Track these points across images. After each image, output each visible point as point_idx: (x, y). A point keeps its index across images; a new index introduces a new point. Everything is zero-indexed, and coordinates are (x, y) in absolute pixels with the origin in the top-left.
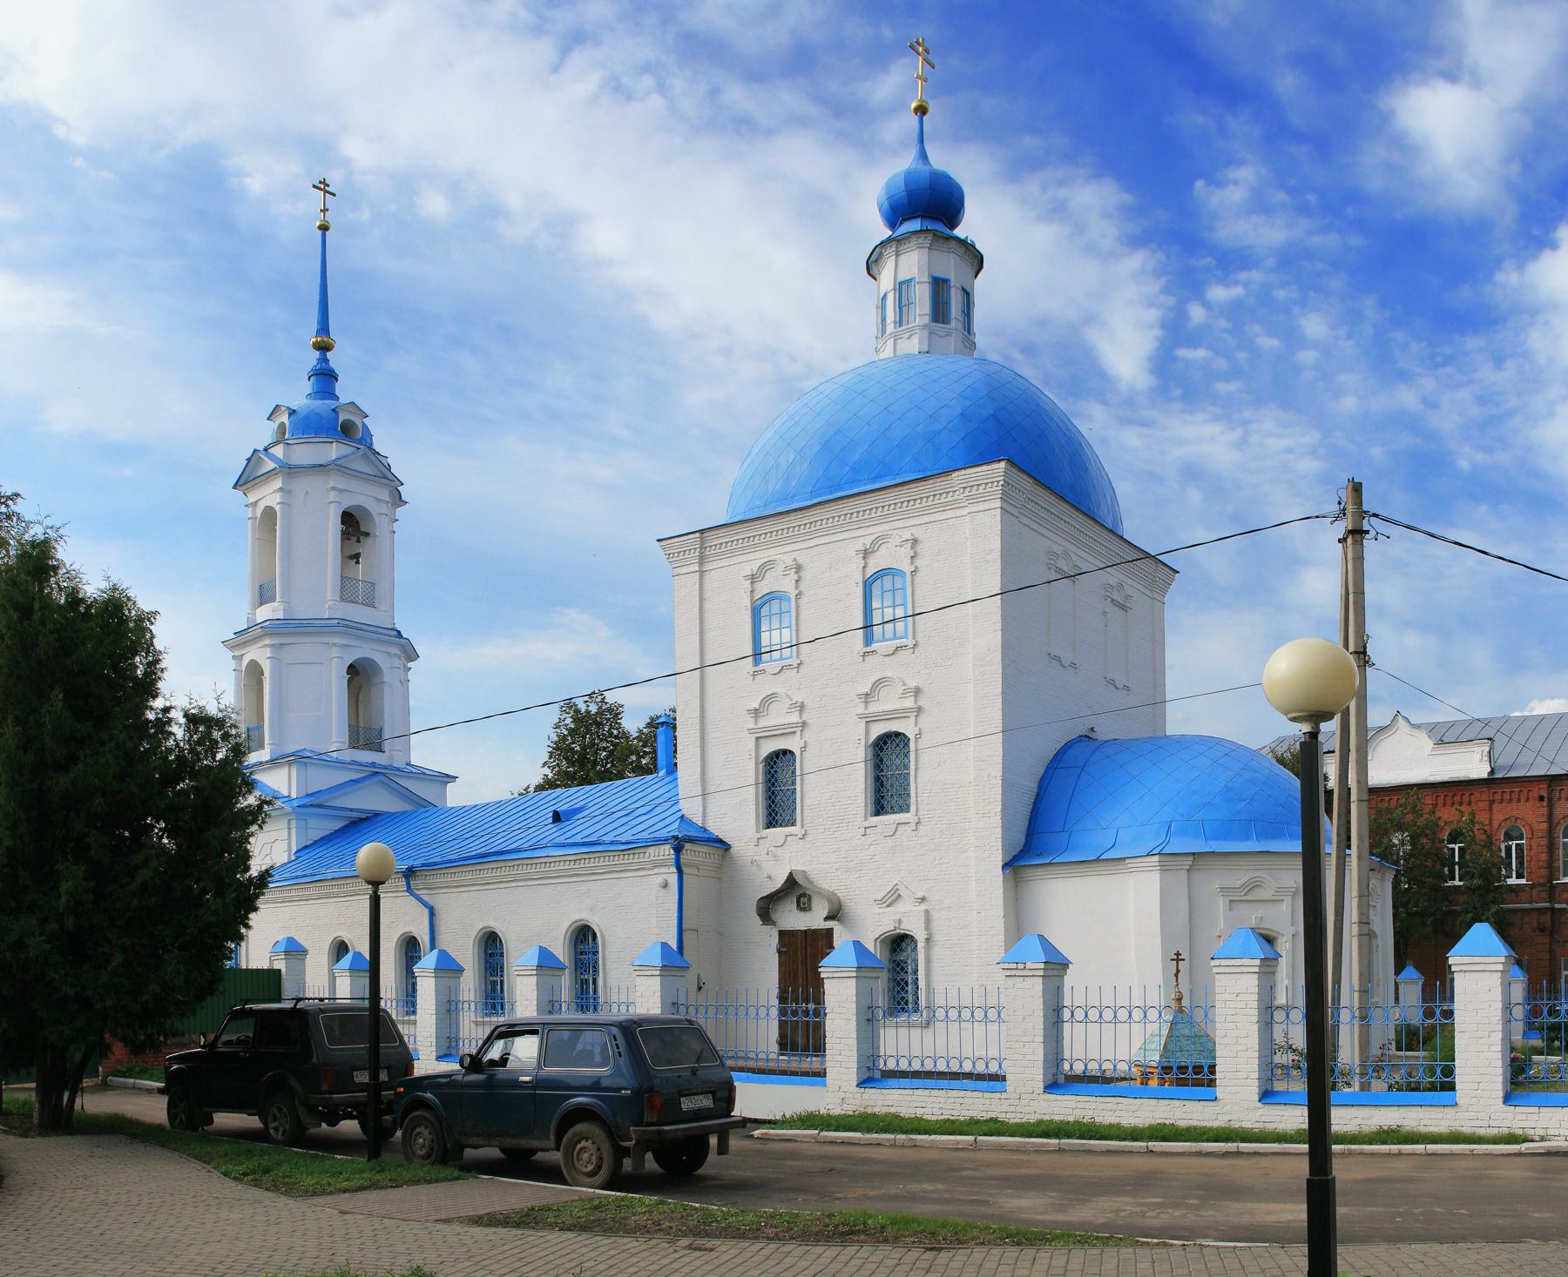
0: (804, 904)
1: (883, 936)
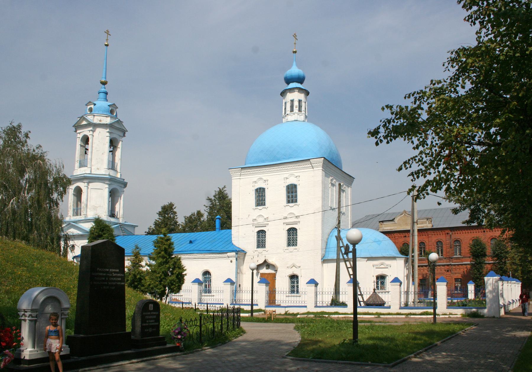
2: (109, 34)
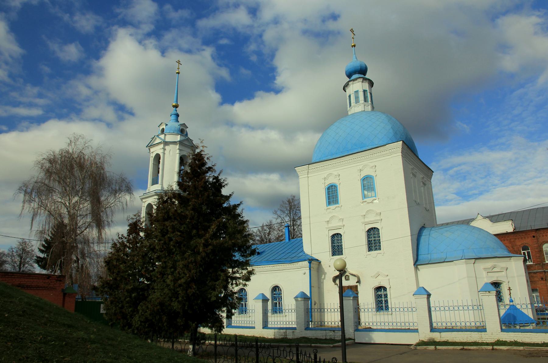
0: (347, 278)
1: (375, 287)
2: (180, 64)
